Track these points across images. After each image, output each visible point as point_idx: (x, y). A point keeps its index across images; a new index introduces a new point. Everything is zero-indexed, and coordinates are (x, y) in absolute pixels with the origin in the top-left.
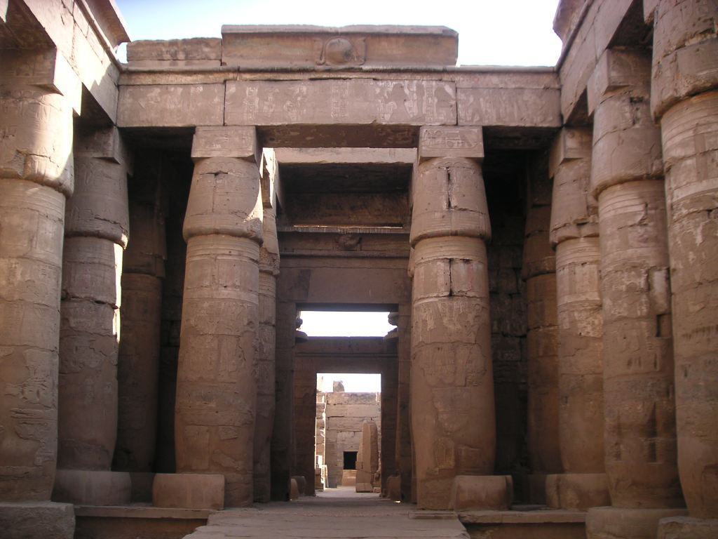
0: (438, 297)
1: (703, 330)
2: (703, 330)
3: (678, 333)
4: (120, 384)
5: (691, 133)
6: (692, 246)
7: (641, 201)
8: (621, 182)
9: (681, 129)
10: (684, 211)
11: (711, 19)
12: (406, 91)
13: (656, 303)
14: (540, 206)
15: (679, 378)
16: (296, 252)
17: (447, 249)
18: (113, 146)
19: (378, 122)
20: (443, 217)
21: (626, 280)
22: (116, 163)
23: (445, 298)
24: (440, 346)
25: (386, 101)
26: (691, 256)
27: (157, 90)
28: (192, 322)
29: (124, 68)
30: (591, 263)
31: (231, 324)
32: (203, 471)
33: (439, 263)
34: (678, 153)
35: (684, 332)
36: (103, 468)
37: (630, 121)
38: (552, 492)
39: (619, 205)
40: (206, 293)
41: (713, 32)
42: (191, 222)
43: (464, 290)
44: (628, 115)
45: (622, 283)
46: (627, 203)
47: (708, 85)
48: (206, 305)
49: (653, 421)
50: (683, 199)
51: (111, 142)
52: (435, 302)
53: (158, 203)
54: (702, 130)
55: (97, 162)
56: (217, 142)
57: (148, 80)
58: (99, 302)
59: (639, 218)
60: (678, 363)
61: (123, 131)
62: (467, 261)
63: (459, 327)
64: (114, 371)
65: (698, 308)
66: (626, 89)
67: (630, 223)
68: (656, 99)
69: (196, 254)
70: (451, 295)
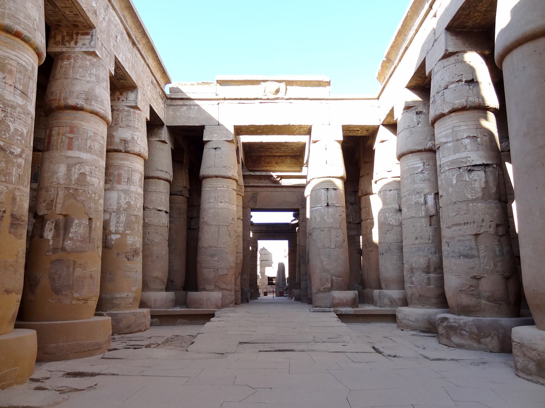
1: (457, 225)
2: (457, 225)
3: (443, 226)
4: (169, 249)
5: (450, 131)
6: (451, 185)
7: (421, 161)
8: (412, 152)
9: (445, 129)
10: (447, 168)
11: (462, 75)
13: (429, 210)
14: (368, 162)
15: (444, 247)
16: (251, 184)
18: (164, 134)
21: (415, 199)
22: (166, 143)
24: (323, 229)
26: (450, 189)
27: (185, 108)
28: (205, 219)
29: (169, 96)
30: (394, 190)
32: (211, 291)
34: (444, 140)
35: (447, 226)
36: (161, 290)
37: (417, 123)
38: (376, 298)
39: (411, 163)
40: (212, 205)
41: (462, 81)
42: (204, 171)
44: (415, 120)
45: (412, 201)
46: (414, 163)
47: (460, 107)
48: (212, 211)
49: (428, 267)
50: (446, 162)
51: (163, 133)
53: (185, 161)
54: (456, 129)
55: (157, 142)
56: (216, 133)
57: (181, 102)
58: (159, 210)
59: (420, 170)
60: (444, 240)
61: (173, 130)
64: (167, 243)
65: (454, 214)
66: (414, 108)
67: (416, 172)
68: (433, 113)
69: (208, 187)
70: (328, 205)
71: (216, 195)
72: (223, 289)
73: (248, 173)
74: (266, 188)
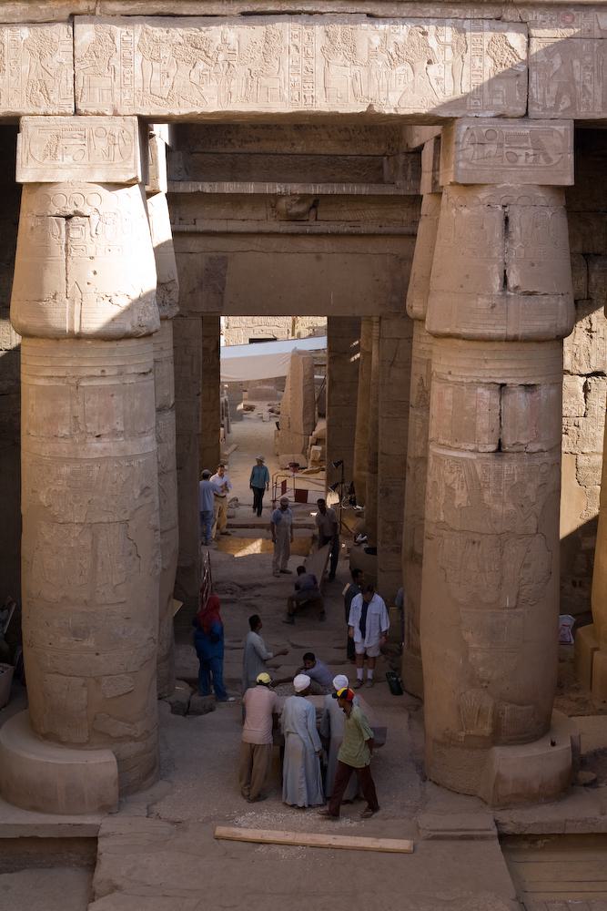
0: (475, 451)
12: (432, 41)
16: (202, 226)
17: (498, 365)
19: (376, 109)
20: (493, 307)
23: (488, 455)
25: (392, 62)
31: (113, 503)
33: (480, 390)
43: (523, 442)
52: (471, 460)
62: (529, 388)
63: (511, 507)
70: (500, 449)
71: (78, 408)
72: (120, 739)
73: (190, 187)
74: (258, 241)
